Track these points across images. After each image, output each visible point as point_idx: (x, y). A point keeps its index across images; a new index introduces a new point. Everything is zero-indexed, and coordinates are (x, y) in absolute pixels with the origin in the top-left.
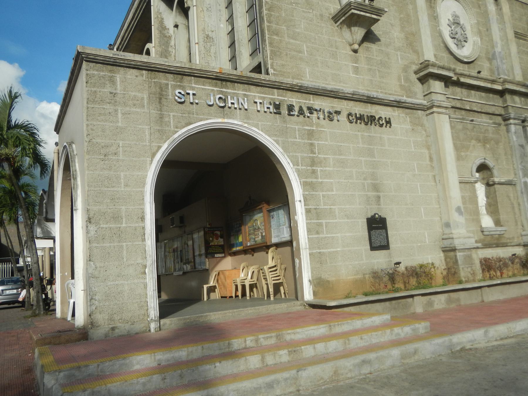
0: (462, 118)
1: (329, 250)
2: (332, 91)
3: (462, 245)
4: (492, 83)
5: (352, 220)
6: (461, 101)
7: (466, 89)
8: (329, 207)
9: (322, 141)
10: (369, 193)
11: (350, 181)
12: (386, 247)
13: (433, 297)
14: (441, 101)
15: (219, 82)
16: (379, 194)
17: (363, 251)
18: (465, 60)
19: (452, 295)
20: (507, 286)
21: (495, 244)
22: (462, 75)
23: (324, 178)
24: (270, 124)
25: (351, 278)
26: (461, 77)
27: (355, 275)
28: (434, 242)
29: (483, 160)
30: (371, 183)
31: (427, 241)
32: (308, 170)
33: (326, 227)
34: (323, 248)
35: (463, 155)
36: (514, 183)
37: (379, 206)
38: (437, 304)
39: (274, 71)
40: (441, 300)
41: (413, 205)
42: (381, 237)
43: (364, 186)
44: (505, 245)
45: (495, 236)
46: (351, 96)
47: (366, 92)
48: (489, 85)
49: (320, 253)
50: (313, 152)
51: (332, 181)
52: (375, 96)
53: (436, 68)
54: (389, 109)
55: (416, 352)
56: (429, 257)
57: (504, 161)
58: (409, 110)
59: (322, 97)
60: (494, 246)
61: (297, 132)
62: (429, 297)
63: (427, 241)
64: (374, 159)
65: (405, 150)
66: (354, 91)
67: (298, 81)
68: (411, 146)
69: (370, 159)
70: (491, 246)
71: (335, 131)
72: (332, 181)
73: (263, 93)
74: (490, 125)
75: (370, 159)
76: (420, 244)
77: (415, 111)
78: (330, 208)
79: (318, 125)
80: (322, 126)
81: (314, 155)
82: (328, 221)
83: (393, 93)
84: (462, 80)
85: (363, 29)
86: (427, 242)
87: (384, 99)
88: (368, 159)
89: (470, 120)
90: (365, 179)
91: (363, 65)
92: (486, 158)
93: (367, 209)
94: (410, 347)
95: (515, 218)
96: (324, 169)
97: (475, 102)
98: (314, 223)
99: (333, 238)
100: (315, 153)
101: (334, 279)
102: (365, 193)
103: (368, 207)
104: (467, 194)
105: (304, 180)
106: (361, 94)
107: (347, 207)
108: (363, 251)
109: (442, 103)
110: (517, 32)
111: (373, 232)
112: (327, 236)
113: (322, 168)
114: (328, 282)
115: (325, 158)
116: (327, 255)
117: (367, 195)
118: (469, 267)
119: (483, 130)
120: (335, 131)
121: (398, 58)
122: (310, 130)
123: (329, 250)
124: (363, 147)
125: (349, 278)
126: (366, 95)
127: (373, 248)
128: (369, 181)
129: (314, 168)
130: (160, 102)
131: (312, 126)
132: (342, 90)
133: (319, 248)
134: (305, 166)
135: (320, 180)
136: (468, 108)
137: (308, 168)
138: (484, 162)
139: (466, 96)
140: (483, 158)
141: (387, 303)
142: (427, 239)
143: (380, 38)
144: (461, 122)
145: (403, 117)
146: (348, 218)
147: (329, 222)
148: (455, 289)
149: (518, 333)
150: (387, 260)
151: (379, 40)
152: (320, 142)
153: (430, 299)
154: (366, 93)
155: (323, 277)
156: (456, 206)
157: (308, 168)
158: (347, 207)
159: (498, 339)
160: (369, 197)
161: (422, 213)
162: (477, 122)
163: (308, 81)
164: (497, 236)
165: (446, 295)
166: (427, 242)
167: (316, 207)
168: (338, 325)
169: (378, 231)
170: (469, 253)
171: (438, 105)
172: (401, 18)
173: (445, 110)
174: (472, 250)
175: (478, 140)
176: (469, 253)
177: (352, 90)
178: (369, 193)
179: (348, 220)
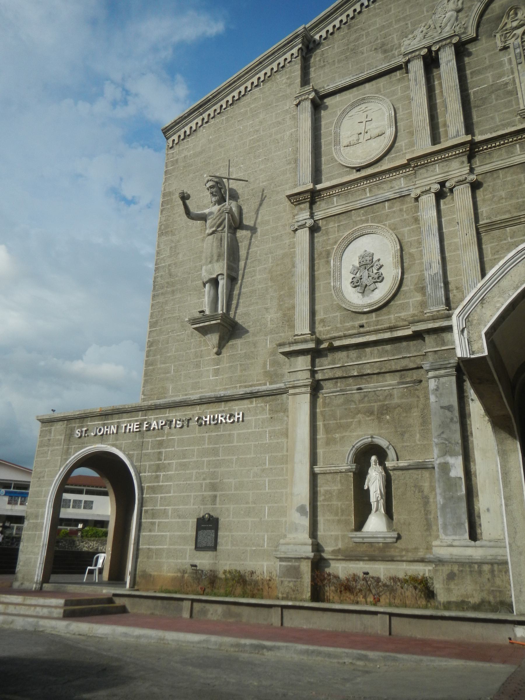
0: (341, 390)
1: (157, 547)
2: (181, 402)
3: (282, 553)
4: (391, 331)
5: (183, 520)
6: (344, 368)
7: (354, 350)
8: (164, 508)
9: (169, 448)
10: (205, 493)
11: (188, 482)
12: (214, 548)
13: (208, 606)
14: (294, 381)
15: (104, 417)
16: (215, 493)
17: (188, 551)
18: (365, 310)
19: (233, 608)
20: (320, 613)
21: (367, 557)
22: (335, 338)
23: (165, 482)
24: (131, 441)
25: (171, 574)
26: (335, 341)
27: (175, 573)
28: (275, 547)
29: (370, 439)
30: (210, 483)
31: (266, 545)
32: (152, 476)
33: (158, 526)
34: (152, 545)
35: (337, 437)
36: (430, 466)
37: (214, 506)
38: (212, 614)
39: (144, 396)
40: (216, 611)
41: (255, 503)
42: (209, 537)
43: (202, 486)
44: (390, 559)
45: (377, 545)
46: (200, 401)
47: (212, 394)
48: (387, 335)
49: (149, 548)
50: (160, 459)
51: (171, 483)
52: (222, 395)
53: (300, 340)
54: (246, 402)
55: (12, 622)
56: (265, 564)
57: (418, 435)
58: (271, 397)
59: (177, 408)
60: (366, 558)
61: (150, 444)
62: (203, 604)
63: (266, 545)
64: (218, 458)
65: (257, 443)
66: (200, 397)
67: (152, 402)
68: (266, 437)
69: (214, 459)
70: (359, 558)
71: (183, 437)
72: (171, 483)
73: (131, 417)
74: (394, 387)
75: (214, 459)
76: (255, 548)
77: (278, 396)
78: (165, 509)
79: (169, 434)
80: (172, 435)
81: (160, 462)
82: (161, 520)
83: (255, 383)
84: (337, 343)
85: (215, 334)
86: (266, 547)
87: (233, 395)
88: (211, 459)
89: (355, 389)
90: (204, 479)
91: (225, 364)
92: (374, 436)
93: (201, 509)
94: (11, 618)
95: (427, 519)
96: (167, 473)
97: (368, 363)
98: (149, 522)
99: (163, 536)
100: (161, 460)
101: (156, 573)
102: (201, 493)
103: (202, 507)
104: (335, 488)
105: (148, 485)
106: (207, 397)
107: (181, 507)
108: (188, 551)
109: (296, 382)
110: (520, 216)
111: (200, 532)
112: (158, 534)
113: (164, 473)
114: (150, 575)
115: (169, 464)
116: (155, 551)
117: (203, 495)
118: (292, 581)
119: (381, 398)
120: (183, 437)
121: (267, 343)
122: (161, 440)
123: (157, 547)
124: (208, 448)
125: (169, 574)
126: (213, 396)
127: (198, 548)
128: (208, 481)
129: (158, 473)
130: (69, 440)
131: (163, 437)
132: (190, 398)
133: (149, 545)
134: (151, 472)
135: (161, 484)
136: (356, 374)
137: (153, 474)
138: (372, 441)
139: (354, 359)
140: (370, 436)
141: (159, 602)
142: (266, 543)
143: (248, 330)
144: (343, 394)
145: (261, 407)
146: (180, 518)
147: (161, 522)
148: (224, 600)
149: (97, 635)
150: (212, 562)
151: (247, 332)
152: (167, 450)
153: (204, 607)
154: (212, 394)
155: (147, 570)
156: (299, 505)
157: (153, 474)
158: (181, 507)
159: (77, 633)
160: (205, 498)
161: (265, 513)
162: (370, 388)
163: (172, 396)
164: (381, 544)
165: (225, 607)
166: (266, 547)
167: (152, 508)
168: (29, 599)
169: (206, 532)
170: (297, 564)
171: (291, 386)
172: (281, 295)
173: (305, 389)
174: (302, 560)
175: (370, 412)
176: (297, 564)
177: (199, 396)
178: (205, 493)
179: (180, 520)
